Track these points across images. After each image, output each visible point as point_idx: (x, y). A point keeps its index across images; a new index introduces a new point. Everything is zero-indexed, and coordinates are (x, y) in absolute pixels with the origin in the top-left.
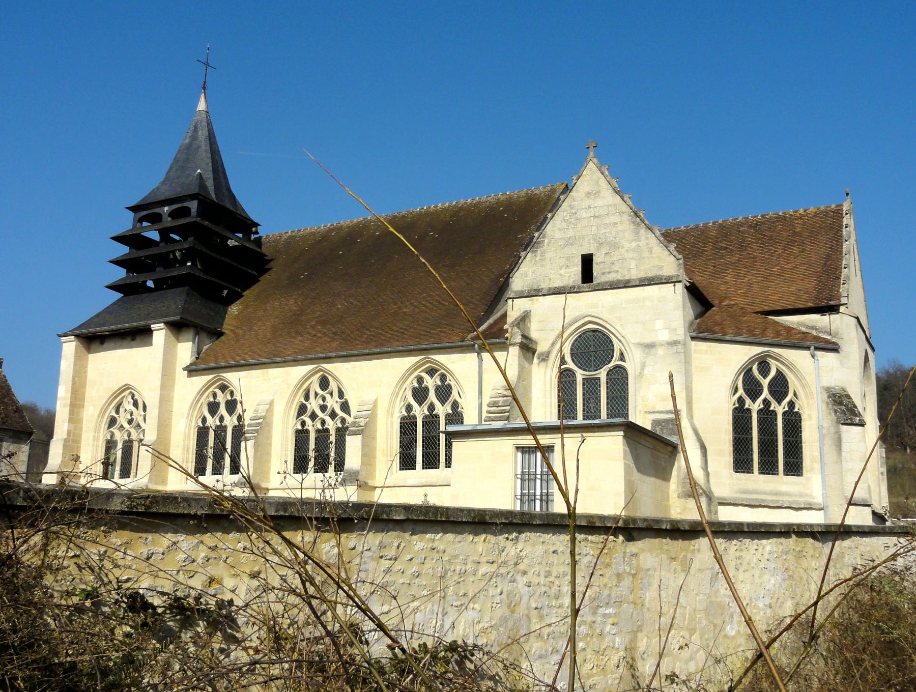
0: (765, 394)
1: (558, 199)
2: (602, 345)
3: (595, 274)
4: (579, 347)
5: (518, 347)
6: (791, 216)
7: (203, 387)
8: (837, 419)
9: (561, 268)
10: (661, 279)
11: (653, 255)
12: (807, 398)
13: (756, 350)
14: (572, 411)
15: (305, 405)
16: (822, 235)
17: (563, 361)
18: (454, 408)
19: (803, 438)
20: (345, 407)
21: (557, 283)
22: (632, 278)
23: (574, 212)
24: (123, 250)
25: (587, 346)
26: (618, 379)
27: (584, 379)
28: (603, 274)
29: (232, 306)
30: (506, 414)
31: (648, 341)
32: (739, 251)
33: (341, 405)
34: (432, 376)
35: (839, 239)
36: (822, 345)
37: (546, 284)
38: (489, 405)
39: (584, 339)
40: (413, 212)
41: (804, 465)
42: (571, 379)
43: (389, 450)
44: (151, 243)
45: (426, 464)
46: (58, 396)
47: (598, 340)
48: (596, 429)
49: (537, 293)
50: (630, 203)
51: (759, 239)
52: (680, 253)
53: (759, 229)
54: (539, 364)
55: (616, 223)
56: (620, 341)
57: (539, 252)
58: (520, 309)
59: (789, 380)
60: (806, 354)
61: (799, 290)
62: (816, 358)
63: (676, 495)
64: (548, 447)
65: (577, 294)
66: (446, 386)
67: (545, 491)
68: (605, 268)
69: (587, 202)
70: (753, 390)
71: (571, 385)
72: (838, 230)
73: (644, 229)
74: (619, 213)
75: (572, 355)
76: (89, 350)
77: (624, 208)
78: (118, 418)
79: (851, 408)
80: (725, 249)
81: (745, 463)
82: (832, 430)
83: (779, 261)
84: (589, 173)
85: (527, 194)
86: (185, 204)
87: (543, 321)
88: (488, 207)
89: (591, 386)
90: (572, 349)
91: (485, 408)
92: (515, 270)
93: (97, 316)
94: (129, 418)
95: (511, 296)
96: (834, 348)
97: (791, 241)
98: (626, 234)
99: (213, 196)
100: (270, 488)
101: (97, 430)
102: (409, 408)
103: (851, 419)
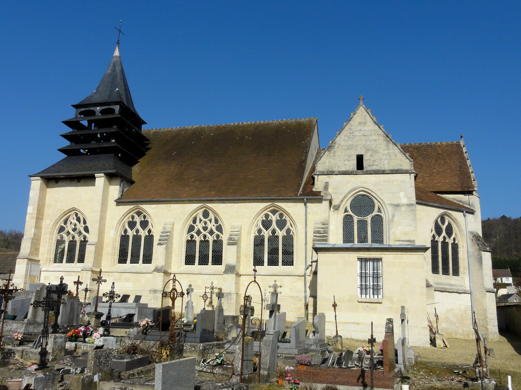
0: (444, 234)
2: (367, 203)
3: (364, 165)
4: (355, 203)
5: (328, 202)
6: (434, 145)
7: (127, 212)
8: (479, 248)
9: (345, 161)
11: (397, 158)
13: (442, 211)
14: (351, 237)
15: (193, 226)
16: (454, 156)
17: (346, 211)
18: (288, 233)
19: (459, 257)
20: (220, 229)
21: (343, 169)
24: (68, 130)
27: (358, 221)
28: (369, 166)
29: (134, 167)
31: (396, 203)
33: (216, 227)
34: (274, 215)
36: (469, 211)
40: (229, 125)
41: (460, 270)
42: (350, 220)
43: (248, 254)
44: (82, 127)
45: (270, 263)
46: (28, 212)
47: (365, 201)
49: (332, 173)
50: (384, 130)
52: (412, 158)
53: (419, 150)
55: (376, 140)
56: (379, 202)
57: (332, 152)
58: (322, 181)
60: (461, 214)
61: (451, 182)
62: (466, 217)
66: (283, 220)
69: (359, 127)
70: (438, 230)
71: (350, 224)
73: (392, 144)
74: (377, 134)
76: (48, 186)
77: (380, 132)
78: (66, 227)
82: (476, 253)
83: (435, 167)
86: (111, 107)
93: (53, 166)
94: (74, 227)
95: (317, 174)
96: (472, 212)
98: (382, 146)
99: (126, 104)
100: (172, 273)
101: (52, 234)
102: (126, 231)
103: (486, 248)
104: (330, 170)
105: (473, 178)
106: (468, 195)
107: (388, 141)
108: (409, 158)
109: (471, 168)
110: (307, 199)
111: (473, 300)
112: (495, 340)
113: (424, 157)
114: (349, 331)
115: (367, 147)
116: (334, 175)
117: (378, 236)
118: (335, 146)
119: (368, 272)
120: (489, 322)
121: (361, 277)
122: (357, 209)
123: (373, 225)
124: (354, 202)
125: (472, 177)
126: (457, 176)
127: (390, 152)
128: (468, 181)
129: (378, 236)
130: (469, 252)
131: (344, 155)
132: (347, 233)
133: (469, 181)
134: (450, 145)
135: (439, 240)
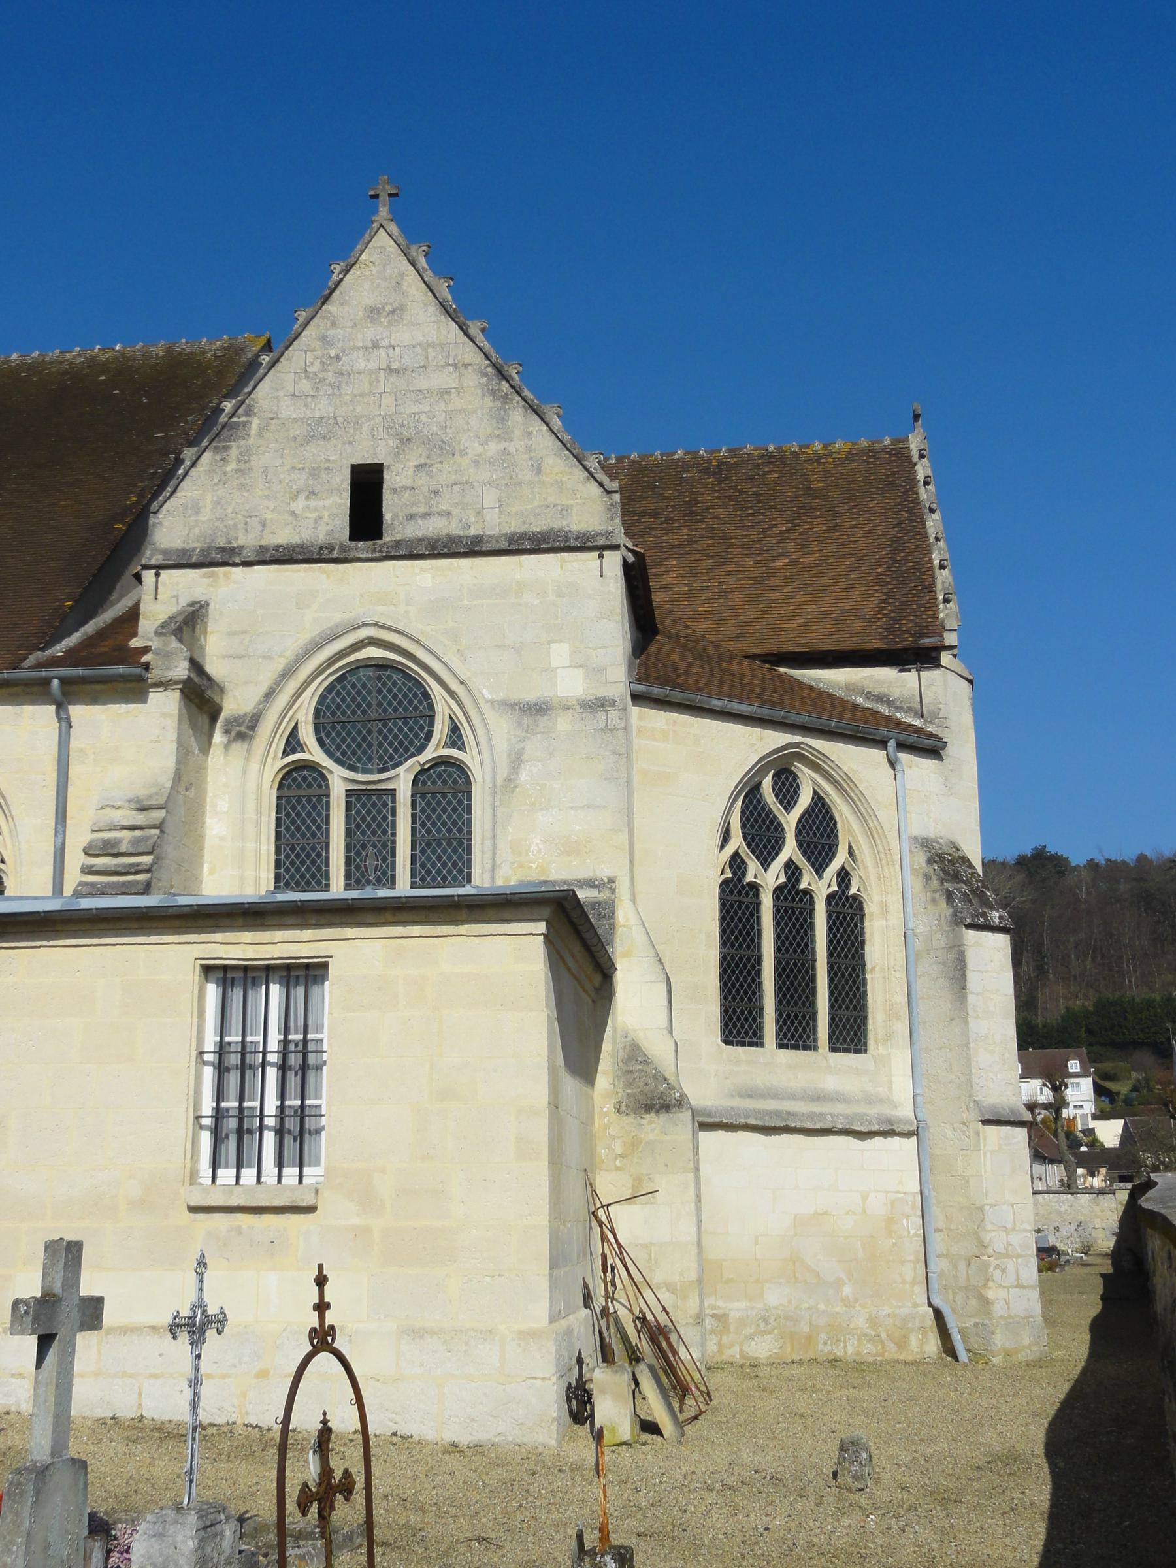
0: (790, 849)
1: (254, 365)
2: (400, 703)
3: (387, 517)
4: (338, 707)
6: (795, 455)
8: (955, 914)
9: (295, 497)
10: (566, 539)
11: (544, 478)
12: (878, 864)
13: (775, 739)
17: (293, 743)
19: (868, 959)
21: (285, 536)
22: (488, 533)
23: (332, 353)
25: (359, 706)
26: (444, 795)
28: (411, 517)
30: (140, 877)
31: (529, 695)
32: (686, 521)
35: (913, 508)
36: (913, 739)
37: (251, 536)
38: (88, 852)
39: (354, 686)
41: (870, 1025)
42: (315, 791)
47: (390, 691)
48: (464, 914)
49: (226, 557)
50: (485, 344)
51: (730, 498)
52: (612, 478)
53: (726, 478)
54: (227, 746)
55: (447, 392)
56: (452, 693)
57: (234, 452)
58: (176, 597)
59: (838, 819)
60: (877, 756)
61: (843, 611)
62: (898, 768)
63: (609, 1107)
64: (307, 966)
65: (341, 567)
67: (293, 1102)
68: (415, 504)
69: (371, 333)
71: (314, 807)
72: (908, 490)
74: (455, 366)
75: (318, 727)
77: (468, 353)
79: (977, 888)
80: (655, 514)
81: (746, 1019)
82: (941, 941)
84: (375, 258)
85: (169, 352)
87: (243, 632)
88: (66, 373)
89: (369, 812)
90: (317, 713)
91: (75, 860)
92: (166, 493)
95: (153, 562)
97: (803, 507)
98: (474, 422)
103: (984, 915)
104: (222, 542)
105: (944, 588)
106: (918, 670)
107: (506, 397)
108: (601, 476)
109: (940, 549)
110: (64, 681)
111: (926, 1164)
112: (1021, 1356)
113: (741, 509)
114: (131, 1376)
115: (402, 425)
116: (236, 565)
117: (444, 865)
118: (246, 424)
119: (256, 1044)
120: (997, 1267)
121: (221, 1069)
122: (349, 733)
123: (423, 811)
124: (333, 700)
125: (939, 586)
126: (877, 584)
127: (512, 449)
128: (920, 606)
129: (444, 865)
130: (909, 933)
131: (293, 468)
132: (298, 856)
133: (923, 605)
134: (862, 452)
135: (764, 879)
